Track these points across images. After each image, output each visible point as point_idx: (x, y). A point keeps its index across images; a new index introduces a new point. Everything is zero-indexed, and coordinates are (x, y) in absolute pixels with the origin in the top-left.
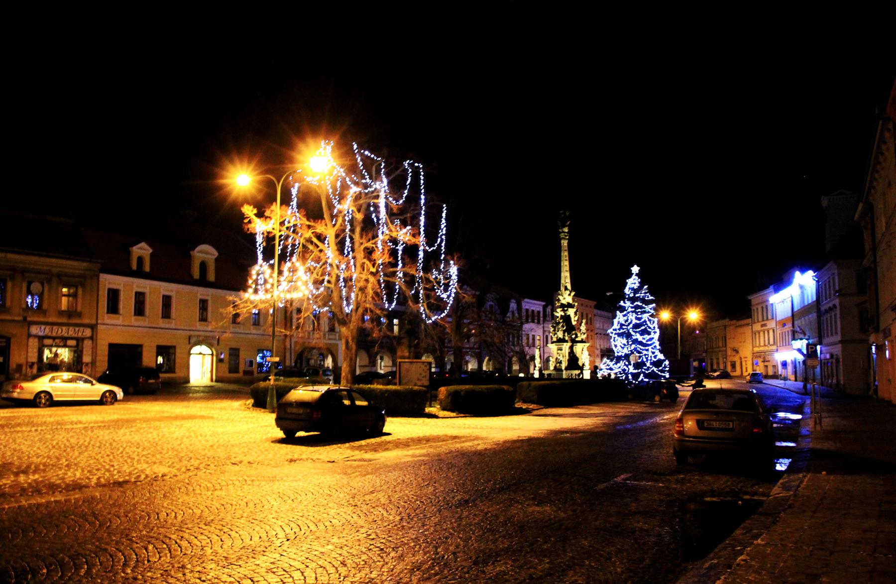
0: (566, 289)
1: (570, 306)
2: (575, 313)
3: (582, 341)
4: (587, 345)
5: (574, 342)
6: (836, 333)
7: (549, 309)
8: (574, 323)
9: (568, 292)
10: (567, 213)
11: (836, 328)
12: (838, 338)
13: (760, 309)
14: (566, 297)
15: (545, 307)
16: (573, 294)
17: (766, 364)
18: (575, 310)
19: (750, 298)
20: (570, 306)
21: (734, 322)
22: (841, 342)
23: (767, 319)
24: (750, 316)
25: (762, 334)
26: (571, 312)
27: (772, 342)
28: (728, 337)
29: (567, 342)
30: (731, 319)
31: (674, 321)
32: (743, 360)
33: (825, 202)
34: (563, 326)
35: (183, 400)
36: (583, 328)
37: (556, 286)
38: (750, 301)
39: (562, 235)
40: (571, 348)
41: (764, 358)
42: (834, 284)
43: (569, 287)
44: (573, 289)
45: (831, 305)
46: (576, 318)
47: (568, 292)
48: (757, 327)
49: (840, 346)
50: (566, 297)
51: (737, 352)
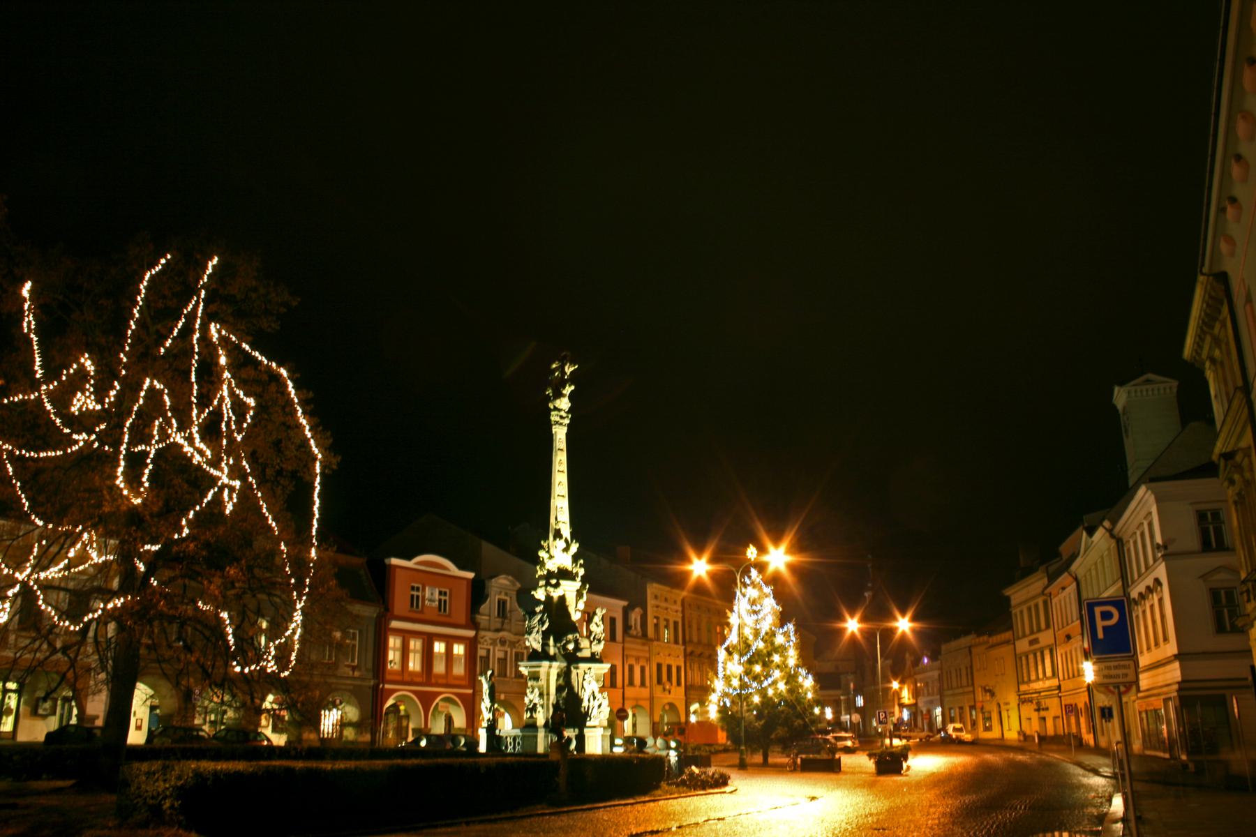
0: (558, 534)
1: (564, 574)
2: (579, 595)
3: (593, 659)
4: (605, 668)
5: (572, 659)
6: (1166, 639)
7: (635, 616)
8: (576, 616)
9: (561, 544)
10: (569, 370)
11: (1163, 616)
12: (1171, 648)
13: (1029, 609)
14: (558, 554)
15: (626, 612)
16: (574, 547)
17: (1043, 713)
18: (577, 584)
19: (1007, 592)
20: (564, 574)
21: (985, 638)
22: (1177, 657)
23: (1039, 630)
24: (1011, 628)
25: (1031, 657)
26: (568, 589)
27: (1049, 673)
28: (977, 665)
29: (552, 659)
30: (979, 635)
31: (869, 635)
32: (1003, 707)
33: (1120, 397)
34: (542, 622)
35: (833, 776)
36: (598, 628)
37: (542, 527)
38: (1008, 599)
39: (554, 417)
40: (565, 675)
41: (1038, 703)
42: (1152, 537)
43: (566, 531)
44: (574, 535)
45: (1149, 581)
46: (581, 605)
47: (561, 544)
48: (1023, 645)
49: (1177, 665)
50: (558, 554)
51: (993, 694)
